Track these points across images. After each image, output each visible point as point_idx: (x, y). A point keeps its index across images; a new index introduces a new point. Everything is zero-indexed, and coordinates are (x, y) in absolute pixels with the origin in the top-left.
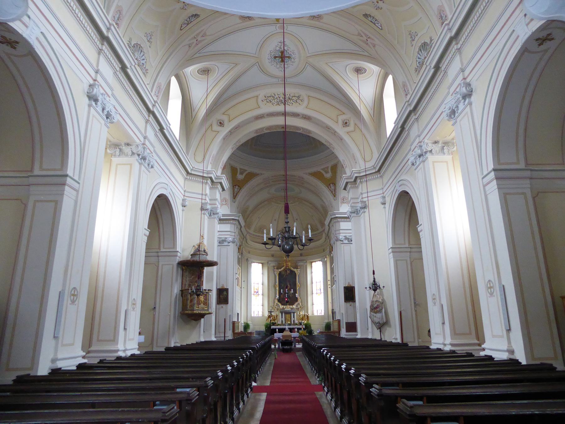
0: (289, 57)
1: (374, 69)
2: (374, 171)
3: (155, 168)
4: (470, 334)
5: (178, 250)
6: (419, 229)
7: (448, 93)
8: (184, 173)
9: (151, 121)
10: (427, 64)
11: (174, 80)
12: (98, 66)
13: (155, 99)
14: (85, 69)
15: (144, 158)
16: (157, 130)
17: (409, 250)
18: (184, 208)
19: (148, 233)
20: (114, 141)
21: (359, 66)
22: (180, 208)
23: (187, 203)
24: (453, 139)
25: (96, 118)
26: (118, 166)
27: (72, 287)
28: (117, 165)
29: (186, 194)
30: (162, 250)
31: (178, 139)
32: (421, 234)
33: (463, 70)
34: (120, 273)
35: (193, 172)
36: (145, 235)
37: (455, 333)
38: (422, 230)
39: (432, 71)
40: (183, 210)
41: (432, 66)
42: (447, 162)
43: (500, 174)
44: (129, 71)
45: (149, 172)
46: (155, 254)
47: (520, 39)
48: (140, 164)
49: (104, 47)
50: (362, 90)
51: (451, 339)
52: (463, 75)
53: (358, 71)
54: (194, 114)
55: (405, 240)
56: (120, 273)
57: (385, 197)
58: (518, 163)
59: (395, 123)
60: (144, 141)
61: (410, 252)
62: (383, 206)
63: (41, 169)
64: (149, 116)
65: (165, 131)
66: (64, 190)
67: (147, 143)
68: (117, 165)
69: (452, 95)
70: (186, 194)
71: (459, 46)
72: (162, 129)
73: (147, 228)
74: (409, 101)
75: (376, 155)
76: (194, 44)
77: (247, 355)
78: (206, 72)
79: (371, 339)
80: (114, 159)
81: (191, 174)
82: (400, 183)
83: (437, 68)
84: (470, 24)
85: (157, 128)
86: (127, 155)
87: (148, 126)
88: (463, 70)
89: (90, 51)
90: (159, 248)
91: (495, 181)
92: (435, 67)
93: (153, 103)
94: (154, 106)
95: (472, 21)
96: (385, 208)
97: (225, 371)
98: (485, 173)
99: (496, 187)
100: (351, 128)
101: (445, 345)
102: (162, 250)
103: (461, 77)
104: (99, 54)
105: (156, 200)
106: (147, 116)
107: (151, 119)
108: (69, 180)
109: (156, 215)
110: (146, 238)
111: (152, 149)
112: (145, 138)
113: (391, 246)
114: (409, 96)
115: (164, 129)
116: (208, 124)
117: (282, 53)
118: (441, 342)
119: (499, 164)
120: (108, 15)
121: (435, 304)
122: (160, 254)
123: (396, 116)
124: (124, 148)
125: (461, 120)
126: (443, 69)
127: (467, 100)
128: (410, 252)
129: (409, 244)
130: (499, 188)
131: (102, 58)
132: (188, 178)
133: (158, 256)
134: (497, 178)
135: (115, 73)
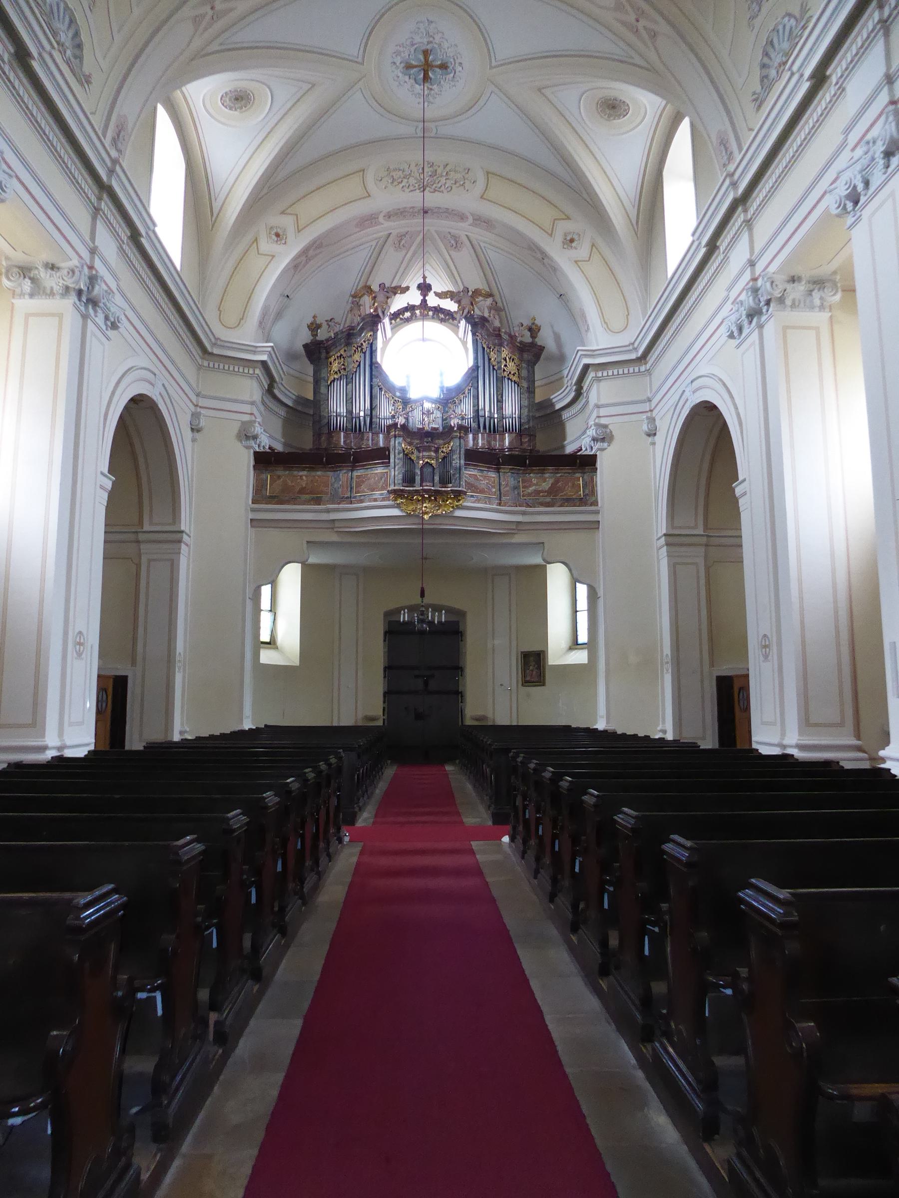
0: (444, 67)
1: (646, 104)
2: (633, 356)
3: (122, 330)
4: (841, 724)
5: (183, 528)
6: (738, 491)
7: (726, 299)
8: (196, 351)
9: (106, 210)
10: (795, 68)
11: (163, 117)
12: (93, 238)
13: (114, 154)
14: (49, 218)
15: (93, 302)
16: (125, 239)
17: (704, 539)
18: (197, 435)
19: (109, 485)
20: (19, 257)
21: (612, 94)
22: (188, 434)
23: (203, 423)
24: (835, 273)
25: (95, 335)
26: (31, 320)
27: (77, 631)
28: (28, 316)
29: (202, 402)
30: (147, 527)
31: (179, 268)
32: (741, 502)
33: (752, 264)
34: (44, 566)
35: (216, 351)
36: (102, 487)
37: (807, 723)
38: (745, 494)
39: (805, 86)
40: (194, 440)
41: (808, 72)
42: (817, 329)
43: (671, 539)
44: (36, 65)
45: (108, 339)
46: (132, 537)
47: (688, 403)
48: (85, 317)
49: (103, 204)
50: (611, 165)
51: (799, 735)
52: (753, 272)
53: (613, 108)
54: (216, 206)
55: (696, 520)
56: (44, 566)
57: (654, 420)
58: (696, 527)
59: (693, 235)
60: (92, 259)
61: (707, 545)
62: (650, 439)
63: (151, 524)
64: (100, 199)
65: (144, 241)
66: (180, 549)
67: (98, 264)
68: (28, 316)
69: (853, 150)
70: (202, 402)
71: (648, 366)
72: (135, 236)
73: (106, 471)
74: (633, 344)
75: (638, 321)
76: (208, 18)
77: (330, 765)
78: (239, 99)
79: (605, 731)
80: (18, 302)
81: (212, 354)
82: (696, 384)
83: (819, 78)
84: (812, 114)
85: (124, 233)
86: (52, 294)
87: (100, 226)
88: (752, 264)
89: (81, 215)
90: (141, 523)
91: (665, 547)
92: (813, 76)
93: (109, 164)
94: (111, 172)
95: (807, 122)
96: (654, 444)
97: (255, 809)
98: (660, 535)
99: (666, 554)
100: (583, 251)
101: (784, 747)
102: (147, 527)
103: (747, 276)
104: (94, 219)
105: (126, 408)
106: (93, 198)
107: (106, 206)
108: (185, 537)
109: (132, 445)
110: (106, 496)
111: (113, 285)
112: (93, 251)
113: (664, 531)
114: (731, 168)
115: (140, 235)
116: (249, 237)
117: (426, 78)
118: (776, 741)
119: (673, 527)
120: (105, 137)
121: (766, 657)
122: (141, 537)
123: (694, 223)
124: (43, 274)
125: (873, 214)
126: (834, 79)
127: (755, 320)
128: (707, 545)
129: (706, 528)
130: (668, 556)
131: (100, 226)
132: (206, 364)
133: (138, 542)
134: (667, 544)
135: (121, 248)
